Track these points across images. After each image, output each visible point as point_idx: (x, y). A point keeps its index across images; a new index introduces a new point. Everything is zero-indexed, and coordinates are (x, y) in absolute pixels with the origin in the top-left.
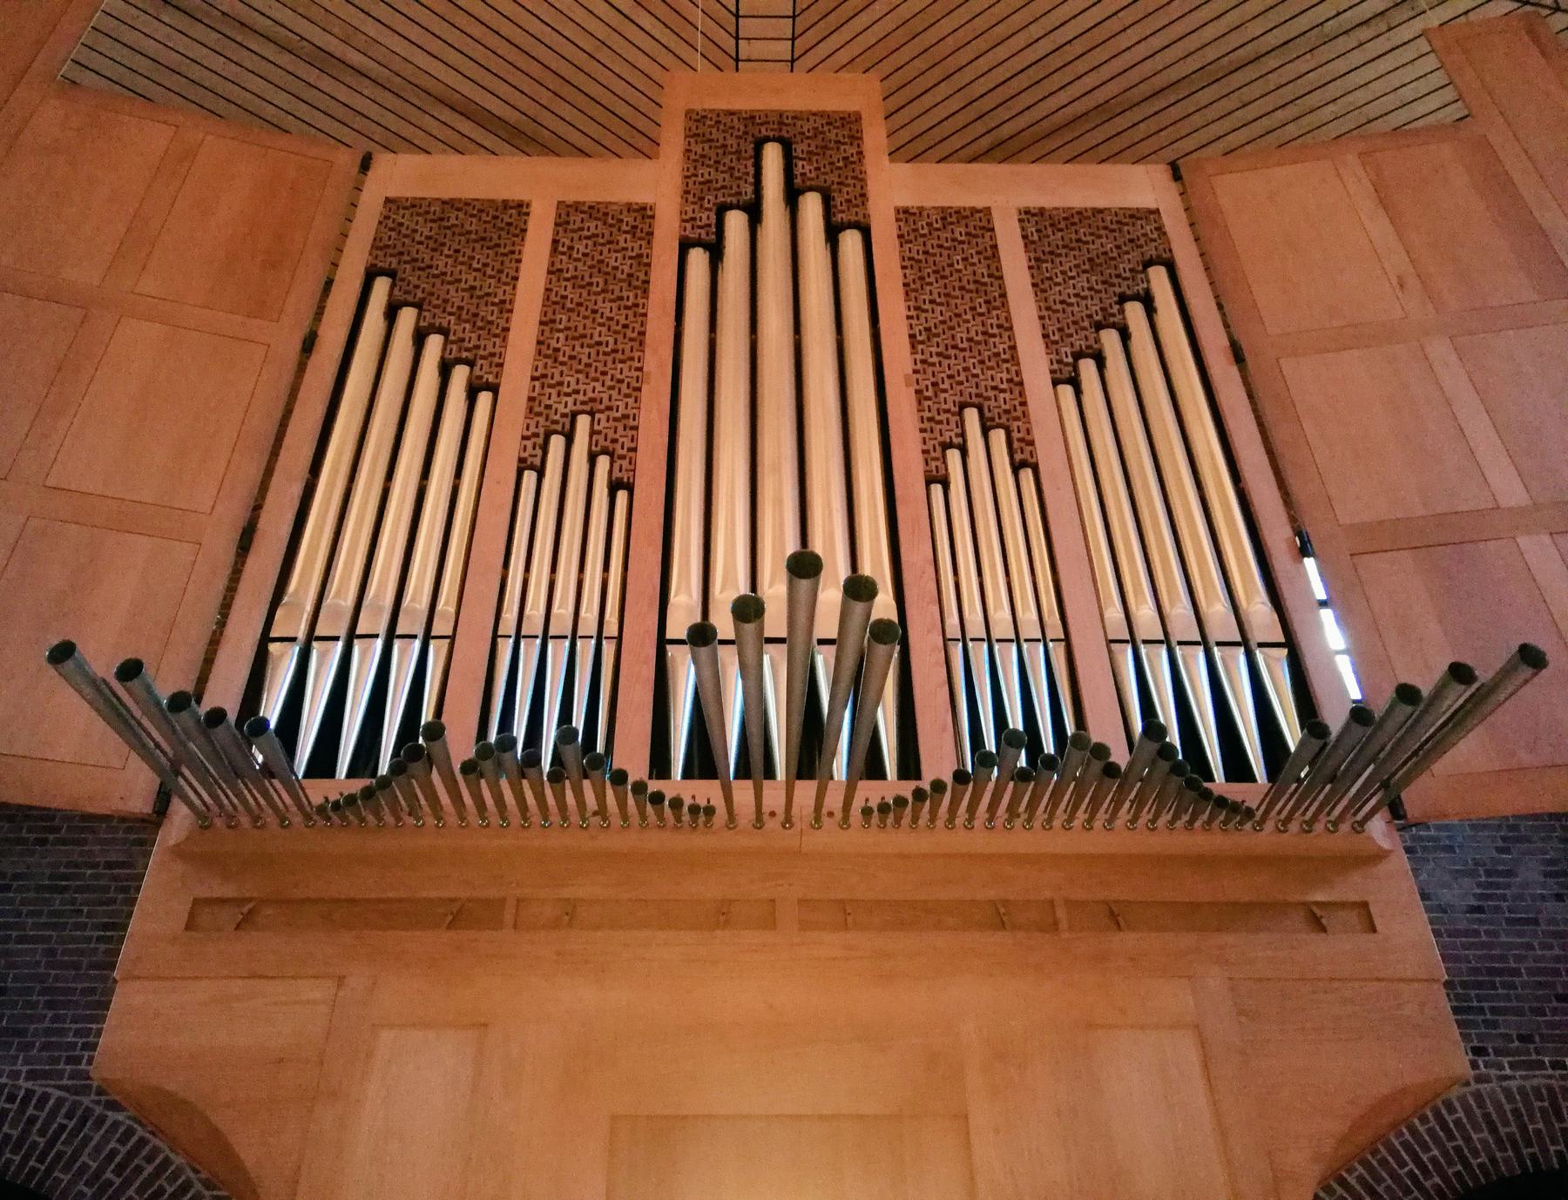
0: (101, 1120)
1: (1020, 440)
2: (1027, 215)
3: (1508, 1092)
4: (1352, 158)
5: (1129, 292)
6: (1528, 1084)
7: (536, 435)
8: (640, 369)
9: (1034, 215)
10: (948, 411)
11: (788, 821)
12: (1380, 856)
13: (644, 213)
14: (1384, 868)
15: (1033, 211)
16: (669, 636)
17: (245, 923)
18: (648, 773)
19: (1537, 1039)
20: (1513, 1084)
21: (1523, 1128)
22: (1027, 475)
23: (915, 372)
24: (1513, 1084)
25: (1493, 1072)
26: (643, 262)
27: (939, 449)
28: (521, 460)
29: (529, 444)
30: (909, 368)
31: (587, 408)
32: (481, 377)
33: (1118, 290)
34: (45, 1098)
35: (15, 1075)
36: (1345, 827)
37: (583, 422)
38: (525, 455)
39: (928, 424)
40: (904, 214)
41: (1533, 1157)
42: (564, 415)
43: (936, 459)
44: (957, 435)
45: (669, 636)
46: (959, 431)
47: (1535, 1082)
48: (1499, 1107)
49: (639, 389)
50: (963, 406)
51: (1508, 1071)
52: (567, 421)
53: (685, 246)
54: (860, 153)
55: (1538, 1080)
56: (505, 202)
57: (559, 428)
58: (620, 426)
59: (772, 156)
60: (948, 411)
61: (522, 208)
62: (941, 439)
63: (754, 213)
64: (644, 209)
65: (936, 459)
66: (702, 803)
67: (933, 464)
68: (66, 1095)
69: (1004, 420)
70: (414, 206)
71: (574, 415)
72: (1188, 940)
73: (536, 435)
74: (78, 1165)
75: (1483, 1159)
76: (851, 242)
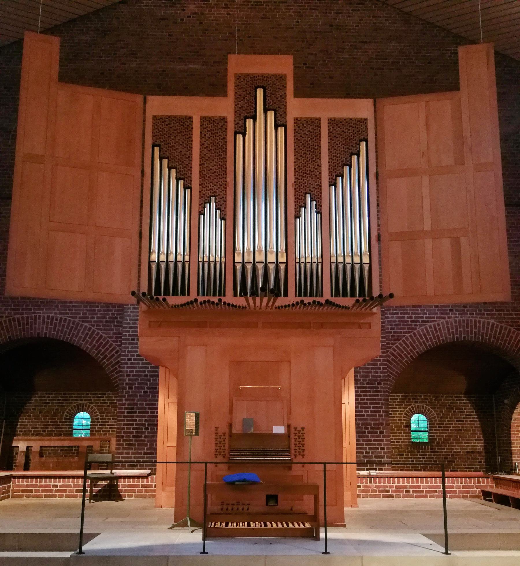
0: (82, 325)
1: (318, 205)
2: (330, 120)
3: (456, 322)
4: (423, 104)
5: (353, 152)
6: (462, 319)
7: (202, 204)
8: (226, 181)
9: (333, 121)
10: (302, 195)
11: (260, 308)
12: (375, 313)
13: (224, 120)
14: (377, 315)
15: (332, 119)
16: (236, 261)
17: (160, 326)
18: (265, 503)
19: (468, 307)
20: (457, 319)
21: (457, 330)
22: (319, 215)
23: (295, 182)
24: (457, 319)
25: (453, 316)
26: (225, 139)
27: (299, 208)
28: (199, 212)
29: (201, 206)
30: (293, 182)
31: (213, 195)
32: (187, 185)
33: (351, 151)
34: (65, 319)
35: (56, 314)
36: (369, 309)
37: (213, 199)
38: (200, 210)
39: (297, 199)
40: (296, 119)
41: (457, 338)
42: (208, 197)
43: (298, 211)
44: (303, 203)
45: (236, 261)
46: (304, 202)
47: (463, 318)
48: (452, 324)
49: (226, 188)
50: (306, 193)
51: (457, 316)
52: (209, 199)
53: (236, 133)
54: (285, 93)
55: (465, 318)
56: (186, 116)
57: (207, 201)
58: (222, 200)
59: (260, 93)
60: (302, 195)
61: (191, 118)
62: (299, 205)
63: (254, 118)
64: (224, 119)
65: (298, 211)
66: (244, 306)
67: (297, 212)
68: (71, 319)
69: (315, 199)
70: (161, 118)
71: (210, 197)
72: (334, 330)
73: (202, 204)
74: (140, 370)
75: (444, 338)
76: (281, 130)
